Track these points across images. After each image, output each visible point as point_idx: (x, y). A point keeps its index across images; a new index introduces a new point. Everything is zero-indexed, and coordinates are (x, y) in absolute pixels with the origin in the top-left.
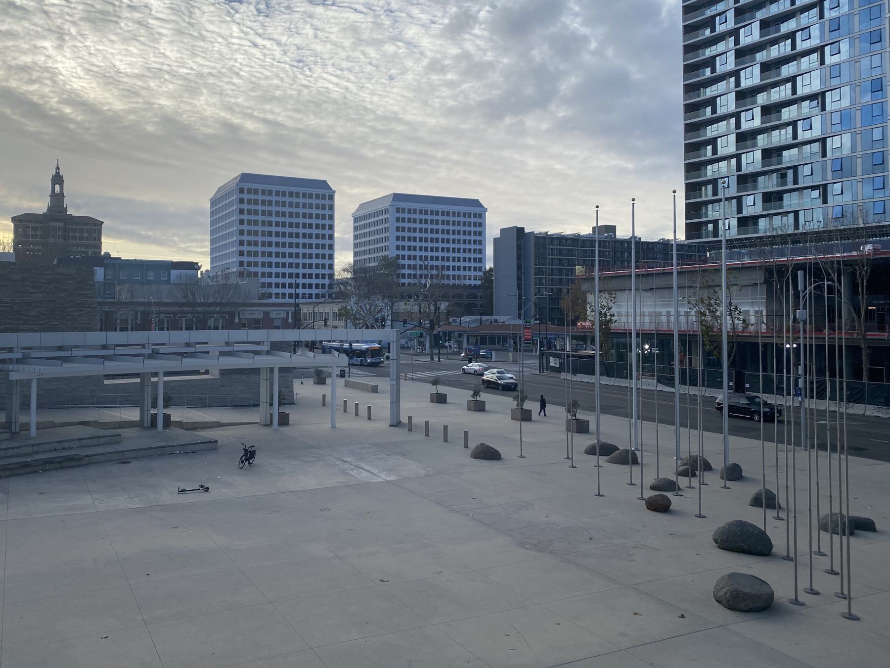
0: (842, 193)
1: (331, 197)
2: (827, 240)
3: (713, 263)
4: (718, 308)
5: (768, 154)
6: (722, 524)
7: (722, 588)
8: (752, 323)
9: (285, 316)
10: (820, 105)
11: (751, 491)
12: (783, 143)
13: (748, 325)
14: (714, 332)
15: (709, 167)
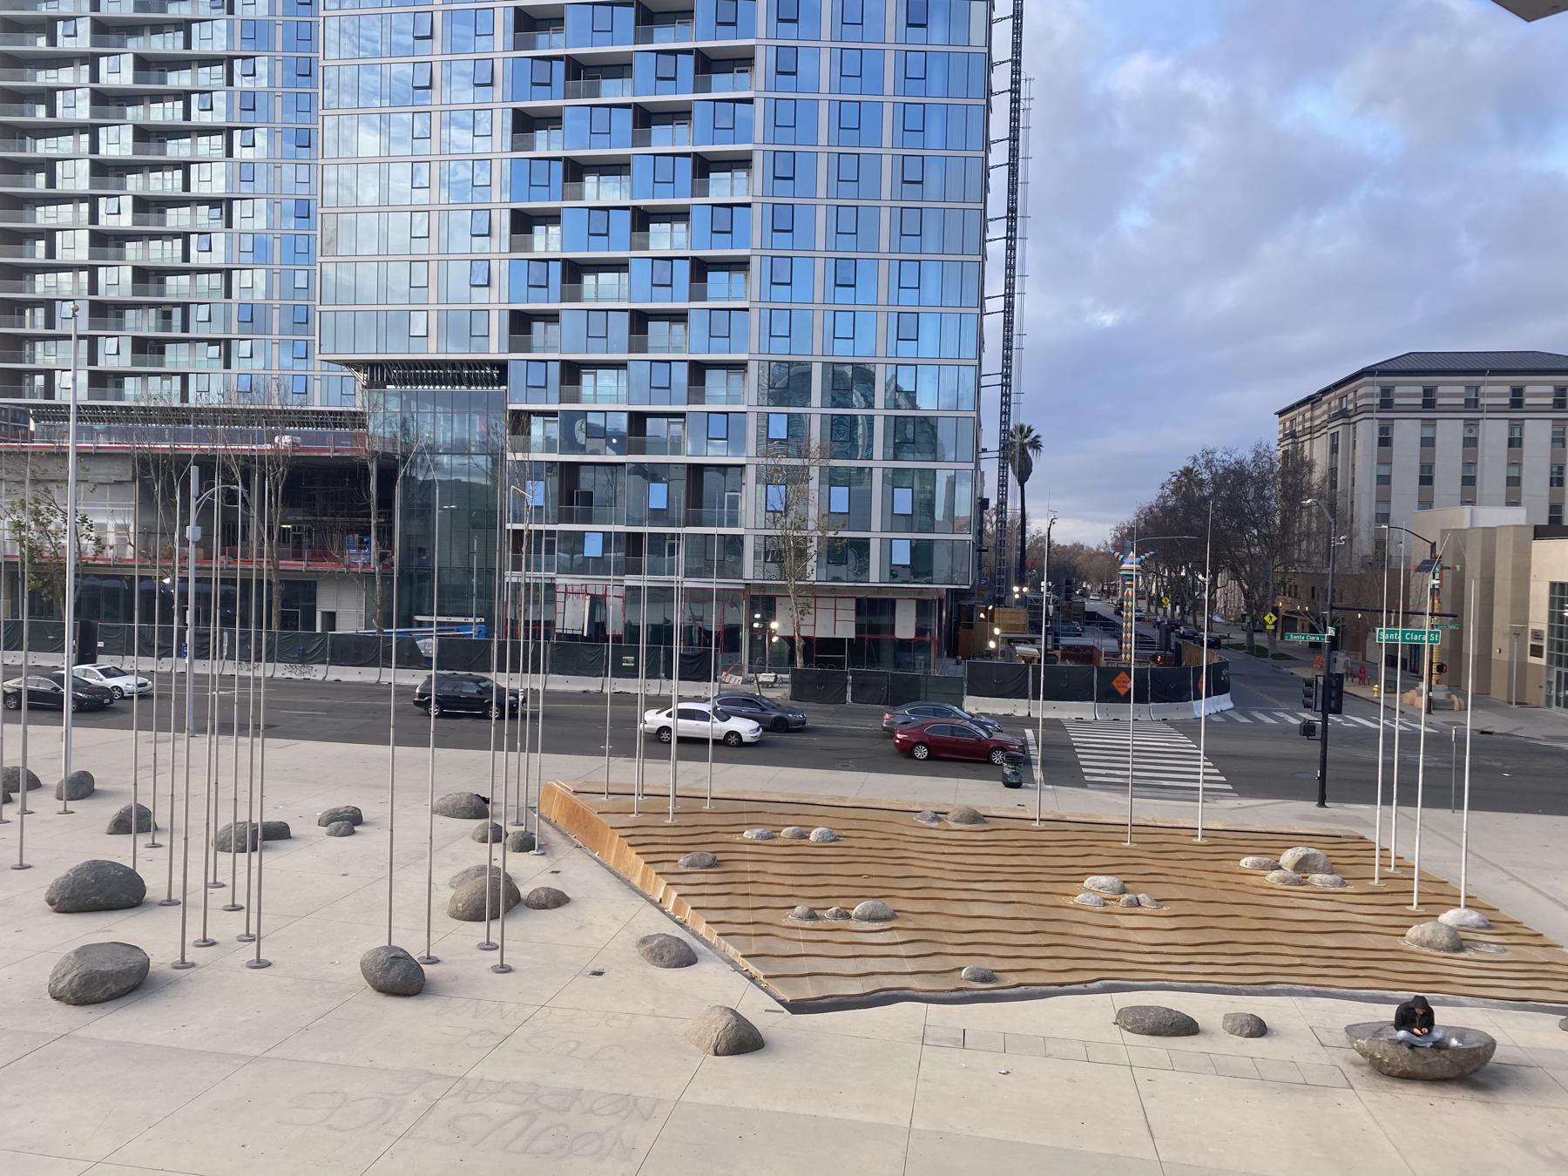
0: (251, 356)
2: (243, 420)
3: (44, 442)
4: (52, 518)
5: (143, 275)
6: (63, 873)
7: (64, 975)
8: (111, 544)
10: (224, 217)
11: (110, 810)
12: (167, 263)
13: (104, 548)
14: (43, 558)
15: (39, 278)
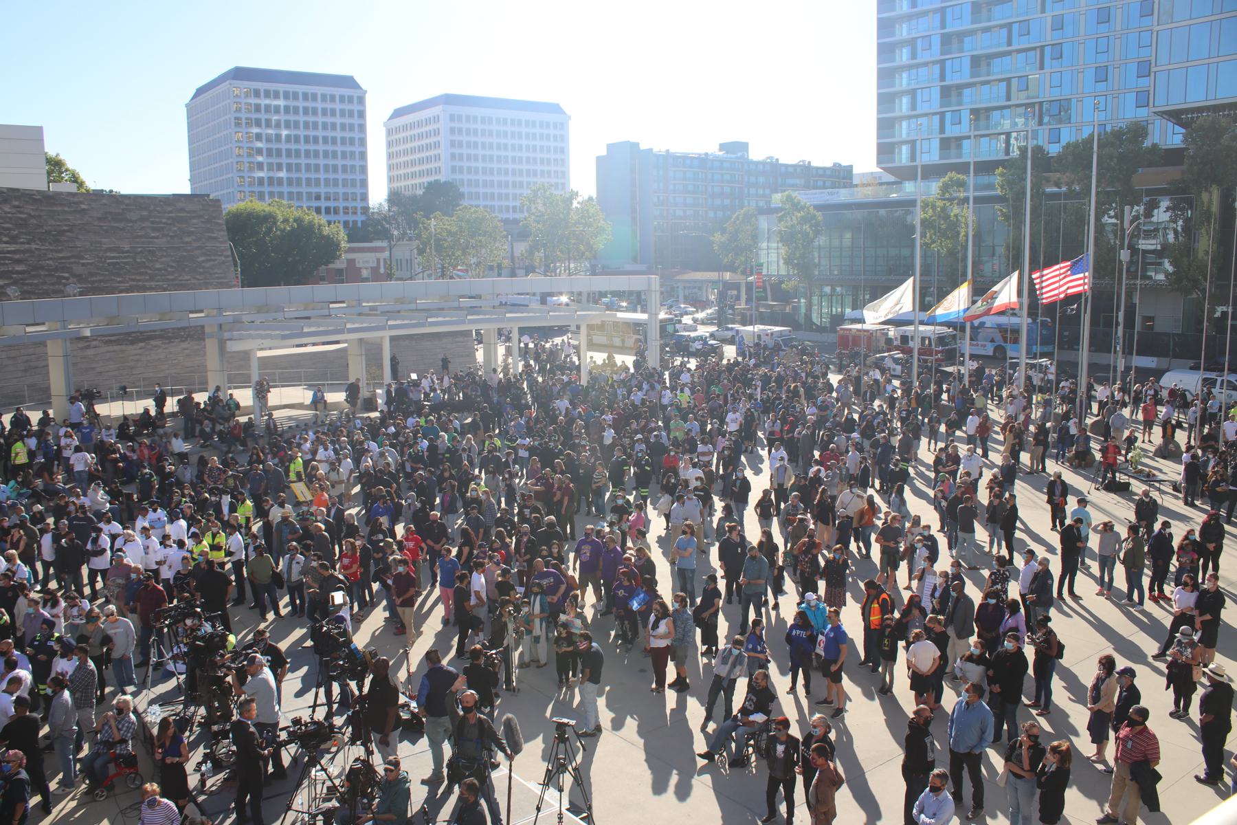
1: (361, 100)
9: (375, 265)
